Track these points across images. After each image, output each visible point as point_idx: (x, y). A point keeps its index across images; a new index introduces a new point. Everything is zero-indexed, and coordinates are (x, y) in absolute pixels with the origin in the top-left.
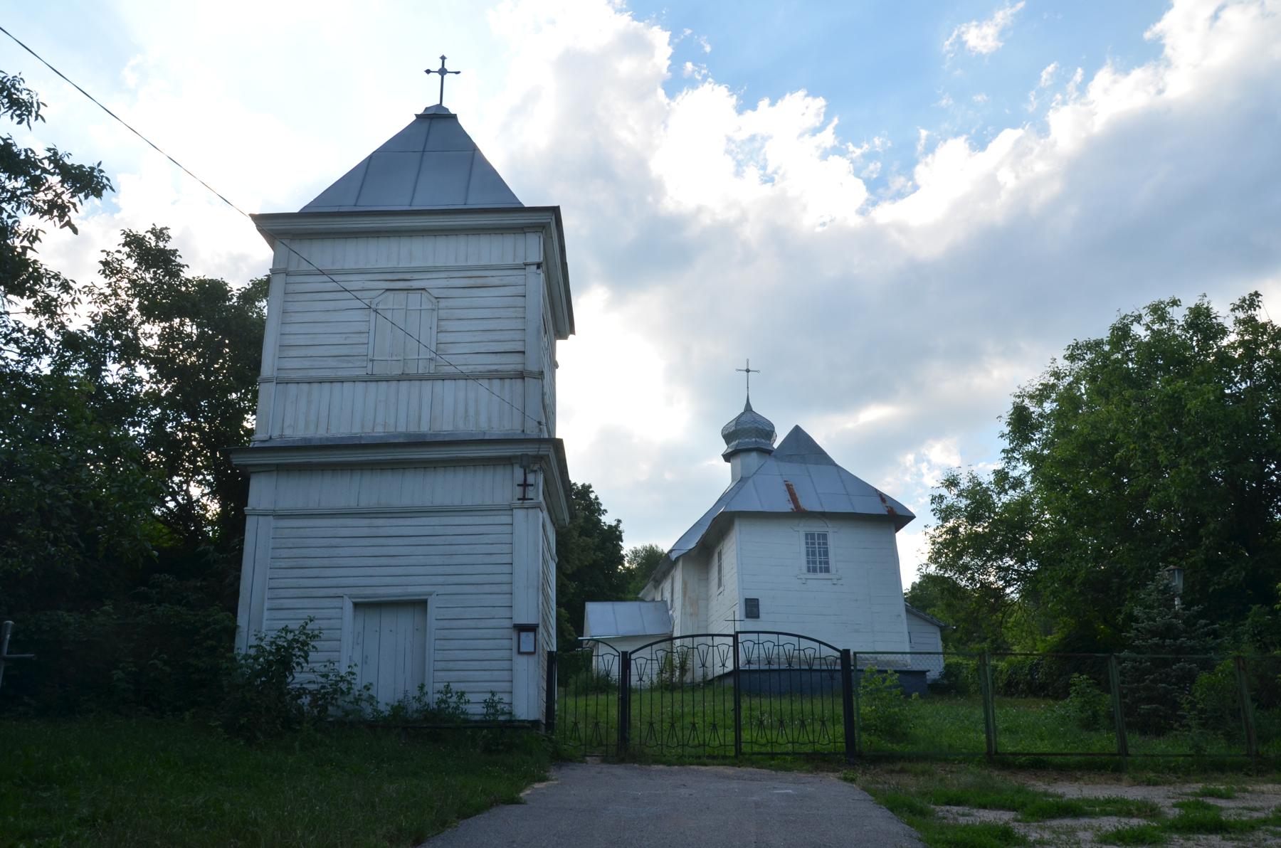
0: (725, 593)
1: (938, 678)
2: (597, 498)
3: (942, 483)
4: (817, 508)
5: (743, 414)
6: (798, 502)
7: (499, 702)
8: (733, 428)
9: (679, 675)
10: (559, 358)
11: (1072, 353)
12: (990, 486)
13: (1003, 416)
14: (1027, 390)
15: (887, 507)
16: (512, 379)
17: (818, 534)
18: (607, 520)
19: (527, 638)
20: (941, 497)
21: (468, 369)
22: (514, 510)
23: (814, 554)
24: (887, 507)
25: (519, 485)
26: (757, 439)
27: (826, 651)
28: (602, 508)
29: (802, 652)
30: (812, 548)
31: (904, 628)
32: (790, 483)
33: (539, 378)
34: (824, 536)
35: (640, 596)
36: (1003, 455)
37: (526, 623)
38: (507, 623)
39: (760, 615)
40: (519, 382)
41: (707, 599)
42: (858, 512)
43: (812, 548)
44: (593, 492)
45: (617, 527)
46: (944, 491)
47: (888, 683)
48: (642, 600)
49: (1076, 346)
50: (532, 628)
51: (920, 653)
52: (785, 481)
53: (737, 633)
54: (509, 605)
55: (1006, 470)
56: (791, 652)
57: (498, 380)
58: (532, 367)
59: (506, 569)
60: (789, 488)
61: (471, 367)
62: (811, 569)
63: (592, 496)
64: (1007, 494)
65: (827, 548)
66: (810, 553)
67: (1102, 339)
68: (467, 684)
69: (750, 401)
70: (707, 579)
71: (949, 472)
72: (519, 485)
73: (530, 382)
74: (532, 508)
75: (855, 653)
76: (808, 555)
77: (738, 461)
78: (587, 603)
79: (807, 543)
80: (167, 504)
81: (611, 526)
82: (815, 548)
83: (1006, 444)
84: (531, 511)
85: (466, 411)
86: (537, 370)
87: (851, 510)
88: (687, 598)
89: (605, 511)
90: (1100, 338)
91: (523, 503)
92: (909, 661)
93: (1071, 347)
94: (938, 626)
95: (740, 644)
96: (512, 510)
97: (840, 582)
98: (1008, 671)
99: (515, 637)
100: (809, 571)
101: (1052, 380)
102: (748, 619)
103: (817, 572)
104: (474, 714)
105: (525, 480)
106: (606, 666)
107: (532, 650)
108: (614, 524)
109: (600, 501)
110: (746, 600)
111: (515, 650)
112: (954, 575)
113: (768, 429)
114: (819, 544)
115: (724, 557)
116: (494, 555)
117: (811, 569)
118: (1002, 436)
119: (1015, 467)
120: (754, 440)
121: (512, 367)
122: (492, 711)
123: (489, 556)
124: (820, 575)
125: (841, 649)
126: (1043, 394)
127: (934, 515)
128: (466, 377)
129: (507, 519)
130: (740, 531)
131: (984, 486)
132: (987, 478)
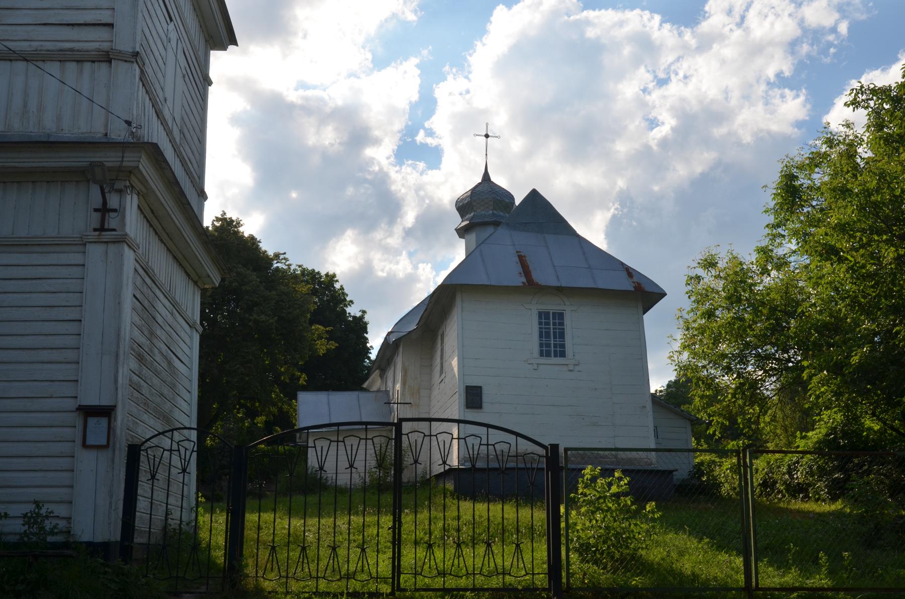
0: (446, 380)
1: (687, 477)
2: (342, 288)
3: (699, 263)
4: (553, 282)
5: (480, 184)
6: (531, 276)
7: (47, 517)
8: (468, 199)
9: (394, 474)
10: (213, 74)
11: (855, 99)
12: (751, 266)
13: (769, 186)
14: (796, 159)
15: (634, 282)
16: (93, 62)
17: (554, 313)
18: (353, 311)
19: (98, 426)
20: (698, 278)
21: (30, 46)
22: (87, 244)
23: (548, 335)
24: (634, 282)
25: (96, 210)
26: (495, 212)
27: (525, 446)
28: (348, 299)
29: (491, 447)
30: (545, 328)
31: (650, 421)
32: (523, 254)
33: (132, 62)
34: (560, 316)
35: (365, 386)
36: (768, 231)
37: (98, 404)
38: (72, 404)
39: (484, 405)
40: (104, 66)
41: (430, 388)
42: (600, 287)
43: (545, 328)
44: (337, 281)
45: (362, 317)
46: (701, 272)
47: (614, 489)
48: (366, 390)
49: (861, 89)
50: (107, 412)
51: (669, 450)
52: (517, 252)
53: (401, 420)
54: (74, 378)
55: (770, 247)
56: (476, 448)
57: (74, 64)
58: (123, 44)
59: (72, 328)
60: (522, 260)
61: (35, 44)
62: (541, 355)
63: (337, 286)
64: (769, 275)
65: (564, 329)
66: (544, 334)
67: (890, 86)
68: (9, 490)
69: (489, 171)
70: (431, 366)
71: (707, 251)
72: (96, 210)
73: (121, 69)
74: (114, 242)
75: (566, 450)
76: (541, 336)
77: (473, 237)
78: (299, 393)
79: (540, 323)
80: (377, 372)
81: (356, 317)
82: (549, 328)
83: (771, 219)
84: (112, 248)
85: (25, 106)
86: (131, 50)
87: (594, 286)
88: (407, 387)
89: (352, 302)
90: (887, 85)
91: (99, 235)
92: (654, 461)
93: (855, 91)
94: (689, 420)
95: (404, 437)
96: (85, 245)
97: (577, 368)
98: (764, 469)
99: (79, 423)
100: (541, 355)
101: (824, 148)
102: (468, 410)
103: (551, 356)
104: (10, 533)
105: (105, 202)
106: (471, 453)
107: (104, 442)
108: (358, 314)
109: (346, 291)
110: (467, 387)
111: (79, 441)
112: (709, 364)
113: (507, 201)
114: (554, 324)
115: (446, 339)
116: (57, 309)
117: (545, 352)
118: (766, 212)
119: (780, 244)
120: (491, 212)
121: (95, 45)
122: (35, 530)
123: (48, 309)
124: (554, 360)
125: (546, 444)
126: (816, 161)
127: (689, 297)
128: (26, 57)
129: (76, 258)
130: (462, 300)
131: (745, 267)
132: (749, 258)
